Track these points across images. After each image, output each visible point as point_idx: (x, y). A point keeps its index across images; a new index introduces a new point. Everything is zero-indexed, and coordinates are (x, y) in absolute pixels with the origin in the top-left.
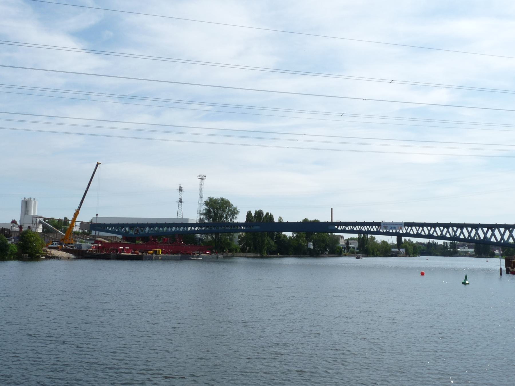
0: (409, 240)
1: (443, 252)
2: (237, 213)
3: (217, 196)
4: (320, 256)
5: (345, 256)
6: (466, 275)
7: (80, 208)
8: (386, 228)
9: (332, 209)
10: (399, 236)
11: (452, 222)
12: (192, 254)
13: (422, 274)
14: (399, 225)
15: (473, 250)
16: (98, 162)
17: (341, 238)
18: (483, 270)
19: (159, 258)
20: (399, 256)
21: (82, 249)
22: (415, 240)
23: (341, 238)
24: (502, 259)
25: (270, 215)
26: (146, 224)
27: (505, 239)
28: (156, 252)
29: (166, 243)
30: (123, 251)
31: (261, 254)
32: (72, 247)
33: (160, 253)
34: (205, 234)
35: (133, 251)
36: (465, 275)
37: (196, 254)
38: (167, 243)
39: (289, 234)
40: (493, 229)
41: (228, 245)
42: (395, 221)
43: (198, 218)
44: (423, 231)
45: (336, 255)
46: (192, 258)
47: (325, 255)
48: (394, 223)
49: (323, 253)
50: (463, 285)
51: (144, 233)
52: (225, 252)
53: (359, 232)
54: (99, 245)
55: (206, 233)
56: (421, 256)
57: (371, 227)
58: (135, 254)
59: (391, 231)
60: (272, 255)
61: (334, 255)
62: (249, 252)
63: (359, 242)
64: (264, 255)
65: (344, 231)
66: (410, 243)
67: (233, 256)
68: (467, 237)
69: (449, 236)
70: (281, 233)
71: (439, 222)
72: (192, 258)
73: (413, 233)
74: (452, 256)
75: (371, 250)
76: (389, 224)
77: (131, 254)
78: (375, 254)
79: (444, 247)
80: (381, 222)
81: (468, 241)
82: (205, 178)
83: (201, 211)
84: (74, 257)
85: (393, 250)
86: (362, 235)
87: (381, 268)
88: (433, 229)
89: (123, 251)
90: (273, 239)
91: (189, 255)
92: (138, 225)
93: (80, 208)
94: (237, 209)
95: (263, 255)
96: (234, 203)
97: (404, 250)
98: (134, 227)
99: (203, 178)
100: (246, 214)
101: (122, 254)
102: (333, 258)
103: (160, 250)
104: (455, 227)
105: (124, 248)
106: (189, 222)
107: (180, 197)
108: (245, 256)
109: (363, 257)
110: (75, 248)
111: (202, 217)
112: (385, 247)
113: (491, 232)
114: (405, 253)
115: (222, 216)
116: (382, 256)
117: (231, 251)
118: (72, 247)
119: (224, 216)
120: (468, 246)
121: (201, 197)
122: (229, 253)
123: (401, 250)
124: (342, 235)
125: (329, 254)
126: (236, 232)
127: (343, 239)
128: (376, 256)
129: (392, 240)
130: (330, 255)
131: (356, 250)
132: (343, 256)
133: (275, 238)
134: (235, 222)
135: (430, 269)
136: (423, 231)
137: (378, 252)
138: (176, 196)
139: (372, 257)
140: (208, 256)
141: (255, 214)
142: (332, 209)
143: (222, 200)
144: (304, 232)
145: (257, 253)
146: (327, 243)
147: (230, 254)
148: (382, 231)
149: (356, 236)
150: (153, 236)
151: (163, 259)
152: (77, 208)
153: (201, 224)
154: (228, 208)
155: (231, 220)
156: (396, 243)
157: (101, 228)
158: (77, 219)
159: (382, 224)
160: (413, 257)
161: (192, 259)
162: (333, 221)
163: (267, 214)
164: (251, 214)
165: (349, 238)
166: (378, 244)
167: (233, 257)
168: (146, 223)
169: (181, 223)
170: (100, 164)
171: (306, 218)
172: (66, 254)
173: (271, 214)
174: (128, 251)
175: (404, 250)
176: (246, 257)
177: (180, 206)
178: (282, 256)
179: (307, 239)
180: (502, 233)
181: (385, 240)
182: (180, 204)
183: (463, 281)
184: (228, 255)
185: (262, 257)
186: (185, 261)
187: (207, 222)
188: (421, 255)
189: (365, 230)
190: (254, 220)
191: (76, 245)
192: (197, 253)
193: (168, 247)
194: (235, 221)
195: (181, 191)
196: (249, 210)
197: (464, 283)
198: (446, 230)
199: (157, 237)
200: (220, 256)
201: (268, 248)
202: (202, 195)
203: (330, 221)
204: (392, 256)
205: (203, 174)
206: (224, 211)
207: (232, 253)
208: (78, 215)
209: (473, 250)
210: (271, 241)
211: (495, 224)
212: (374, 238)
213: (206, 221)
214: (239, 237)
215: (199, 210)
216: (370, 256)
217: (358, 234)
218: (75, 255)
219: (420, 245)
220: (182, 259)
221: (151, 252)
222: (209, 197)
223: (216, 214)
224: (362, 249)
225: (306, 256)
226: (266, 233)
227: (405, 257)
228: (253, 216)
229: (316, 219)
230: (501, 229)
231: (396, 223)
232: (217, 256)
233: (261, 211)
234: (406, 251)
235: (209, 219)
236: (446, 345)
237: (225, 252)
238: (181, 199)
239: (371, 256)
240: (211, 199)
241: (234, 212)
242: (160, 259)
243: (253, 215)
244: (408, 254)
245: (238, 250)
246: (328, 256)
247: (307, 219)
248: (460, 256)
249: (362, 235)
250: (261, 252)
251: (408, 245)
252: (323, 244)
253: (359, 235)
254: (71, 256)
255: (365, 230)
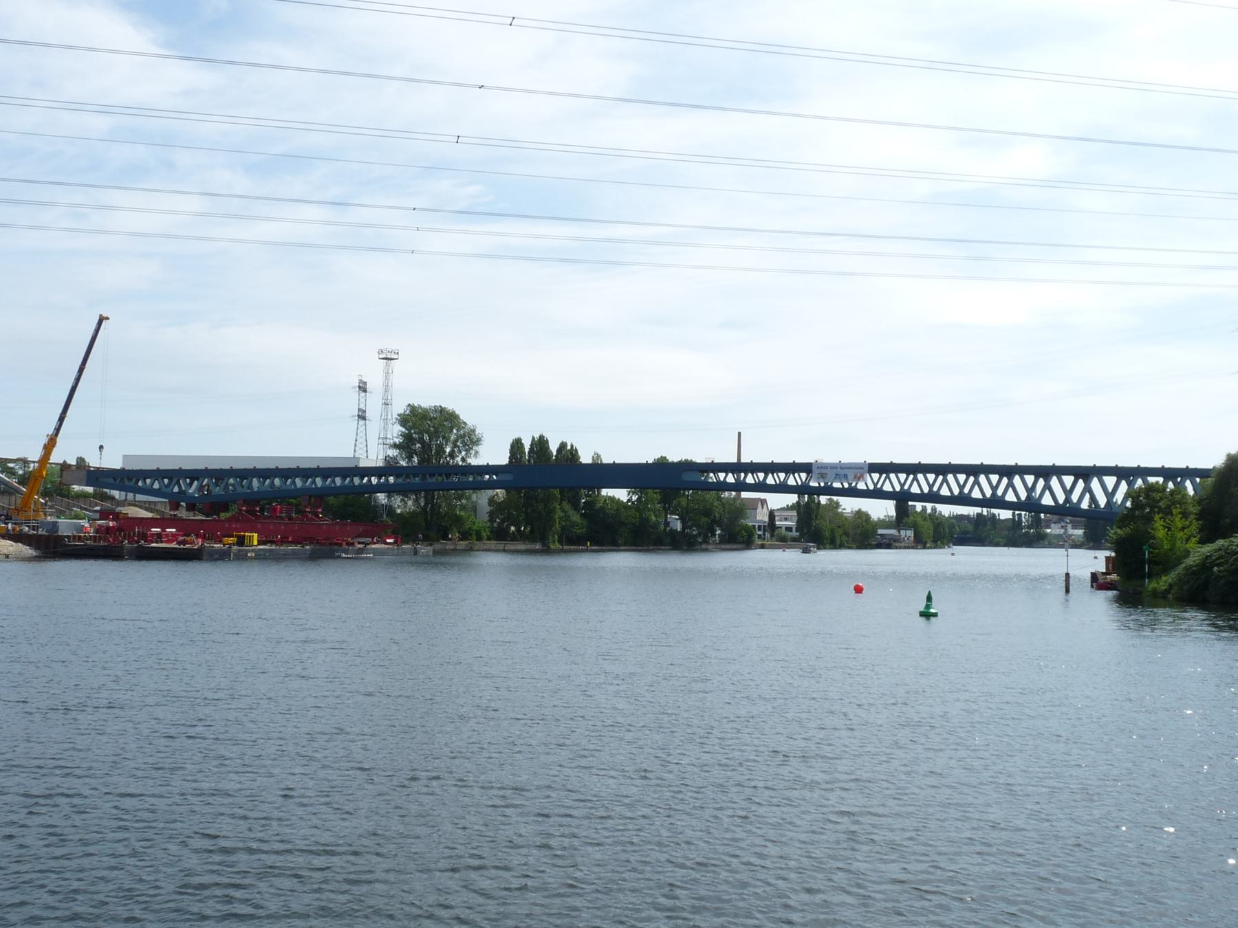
0: (932, 509)
1: (1014, 536)
2: (477, 442)
3: (427, 402)
4: (699, 547)
5: (762, 547)
6: (929, 593)
7: (58, 430)
8: (822, 476)
9: (739, 434)
10: (902, 498)
11: (1058, 464)
12: (344, 543)
13: (858, 590)
14: (857, 468)
15: (1080, 532)
16: (101, 315)
17: (760, 505)
18: (1020, 578)
19: (249, 555)
20: (897, 548)
21: (60, 534)
22: (946, 510)
23: (760, 505)
24: (1069, 550)
25: (569, 447)
26: (314, 469)
27: (1100, 503)
28: (241, 541)
29: (278, 517)
30: (159, 538)
31: (544, 545)
32: (33, 528)
33: (255, 543)
34: (399, 492)
35: (181, 538)
36: (927, 594)
37: (356, 544)
38: (281, 518)
39: (622, 494)
40: (1179, 479)
41: (458, 520)
42: (847, 459)
43: (381, 457)
44: (1010, 489)
45: (739, 546)
46: (344, 555)
47: (710, 547)
48: (844, 464)
49: (706, 541)
50: (924, 618)
51: (249, 491)
52: (451, 539)
53: (799, 490)
54: (111, 524)
55: (403, 491)
56: (954, 547)
57: (884, 476)
58: (187, 546)
59: (837, 485)
60: (572, 547)
61: (735, 546)
62: (514, 538)
63: (798, 513)
64: (552, 547)
65: (761, 487)
66: (935, 518)
67: (469, 550)
68: (1061, 501)
69: (1053, 504)
70: (599, 493)
71: (1023, 462)
72: (344, 555)
73: (919, 492)
74: (1033, 547)
75: (827, 534)
76: (832, 468)
77: (177, 546)
78: (838, 543)
79: (1015, 524)
80: (811, 464)
81: (1066, 511)
82: (396, 356)
83: (386, 438)
84: (34, 554)
85: (880, 531)
86: (806, 496)
87: (771, 575)
88: (1041, 482)
89: (159, 538)
90: (575, 506)
91: (336, 547)
92: (232, 472)
93: (58, 430)
94: (477, 433)
95: (549, 547)
96: (468, 416)
97: (910, 533)
98: (223, 479)
99: (393, 357)
100: (509, 447)
101: (154, 545)
102: (489, 553)
103: (256, 535)
104: (902, 472)
105: (163, 530)
106: (361, 466)
107: (362, 407)
108: (502, 548)
109: (819, 548)
110: (40, 532)
111: (393, 453)
112: (863, 526)
113: (1127, 487)
114: (912, 539)
115: (441, 450)
116: (855, 546)
117: (465, 536)
118: (33, 528)
119: (448, 450)
120: (1071, 522)
121: (386, 404)
122: (461, 542)
123: (903, 532)
124: (762, 498)
125: (721, 542)
126: (482, 489)
127: (765, 506)
128: (841, 546)
129: (881, 510)
130: (723, 547)
131: (795, 534)
132: (756, 549)
133: (582, 505)
134: (473, 464)
135: (875, 577)
136: (976, 486)
137: (844, 538)
138: (352, 402)
139: (830, 549)
140: (388, 548)
141: (531, 445)
142: (739, 434)
143: (442, 410)
144: (654, 488)
145: (534, 541)
146: (715, 516)
147: (463, 544)
148: (817, 485)
149: (792, 499)
150: (245, 501)
151: (261, 557)
152: (51, 431)
153: (389, 468)
154: (455, 431)
155: (463, 460)
156: (893, 513)
157: (115, 480)
158: (51, 458)
159: (814, 468)
160: (935, 548)
161: (345, 558)
162: (743, 460)
163: (563, 446)
164: (522, 444)
165: (788, 506)
166: (846, 518)
167: (472, 553)
168: (252, 467)
169: (204, 468)
170: (107, 318)
171: (664, 456)
172: (12, 546)
173: (572, 446)
174: (173, 537)
175: (910, 533)
176: (504, 551)
177: (362, 429)
178: (598, 548)
179: (664, 507)
180: (994, 485)
181: (864, 509)
182: (362, 422)
183: (922, 610)
184: (458, 548)
185: (546, 551)
186: (325, 561)
187: (404, 465)
188: (954, 545)
189: (867, 486)
190: (529, 461)
191: (43, 524)
192: (359, 543)
193: (272, 527)
194: (473, 461)
195: (365, 391)
196: (1225, 454)
197: (926, 615)
198: (1043, 483)
199: (257, 502)
200: (424, 549)
201: (563, 528)
202: (389, 398)
203: (735, 461)
204: (879, 546)
205: (391, 347)
206: (447, 439)
207: (467, 542)
208: (55, 449)
209: (1080, 532)
210: (571, 512)
211: (1092, 465)
212: (837, 505)
213: (403, 463)
214: (491, 501)
215: (382, 436)
216: (825, 548)
217: (796, 495)
218: (37, 548)
219: (954, 521)
220: (314, 557)
221: (231, 540)
222: (409, 405)
223: (426, 447)
224: (805, 531)
225: (663, 548)
226: (557, 492)
227: (913, 548)
228: (527, 450)
229: (689, 459)
230: (1064, 477)
231: (849, 464)
232: (415, 548)
233: (541, 437)
234: (915, 536)
235: (410, 458)
236: (693, 791)
237: (451, 539)
238: (365, 412)
239: (828, 546)
240: (413, 409)
241: (470, 440)
242: (251, 558)
243: (527, 449)
244: (920, 542)
245: (484, 534)
246: (719, 546)
247: (665, 458)
248: (1051, 545)
249: (806, 496)
250: (543, 539)
251: (919, 520)
252: (704, 520)
253: (799, 497)
254: (26, 551)
255: (867, 486)
